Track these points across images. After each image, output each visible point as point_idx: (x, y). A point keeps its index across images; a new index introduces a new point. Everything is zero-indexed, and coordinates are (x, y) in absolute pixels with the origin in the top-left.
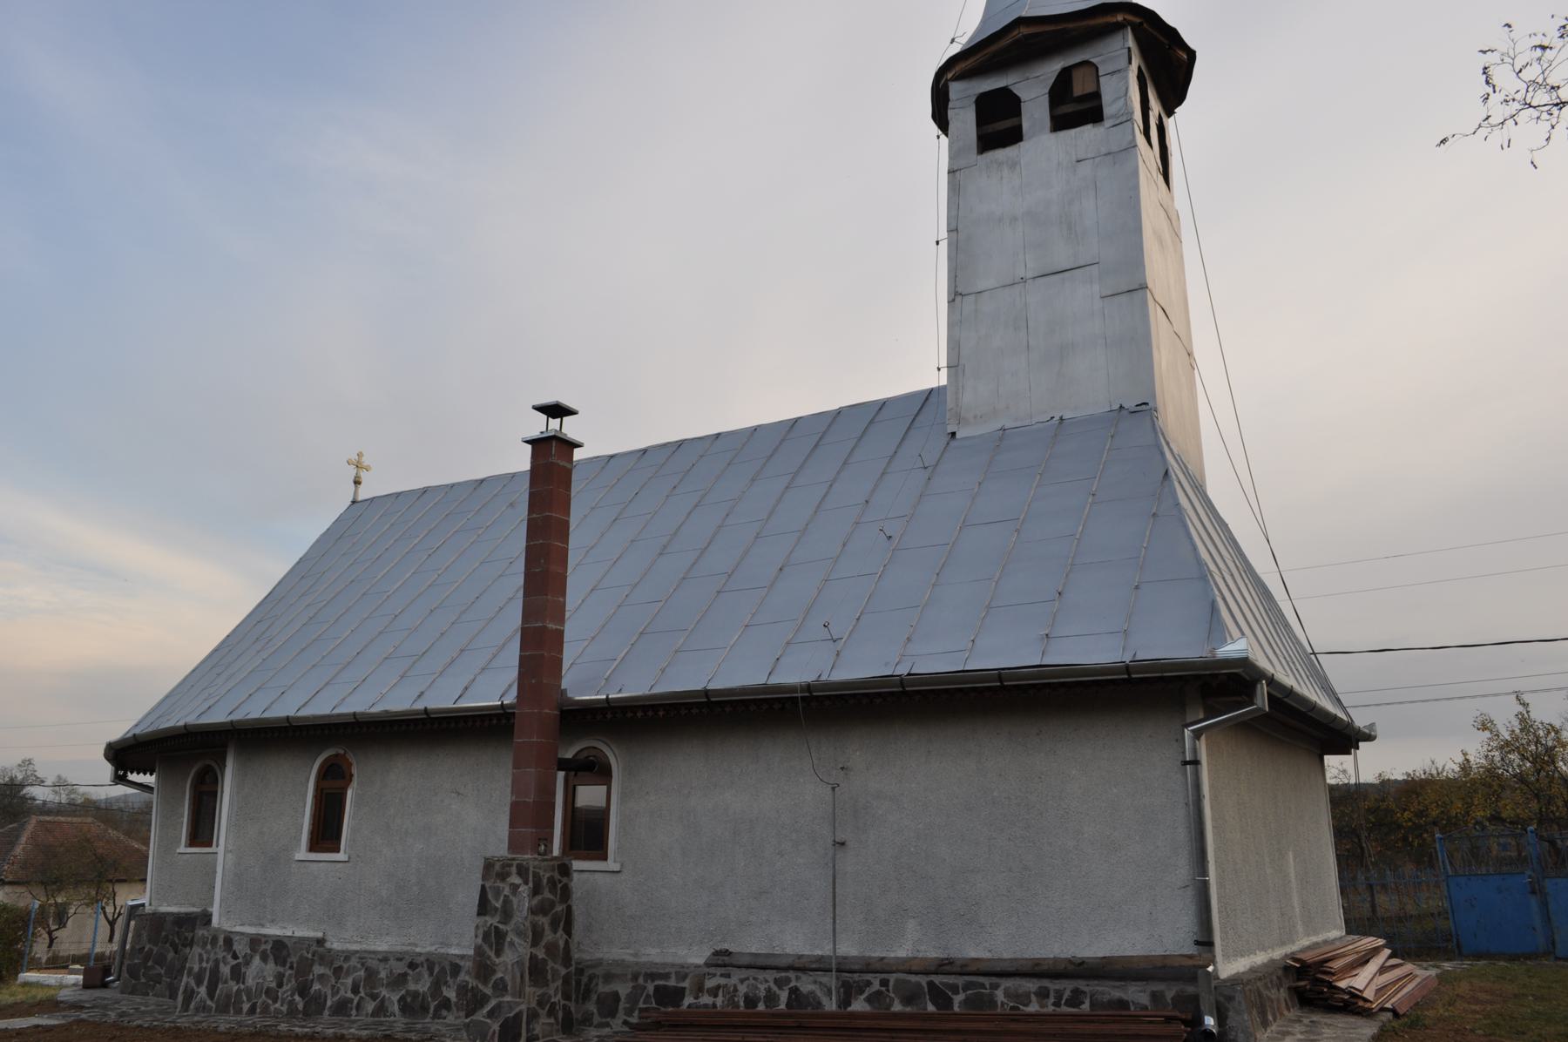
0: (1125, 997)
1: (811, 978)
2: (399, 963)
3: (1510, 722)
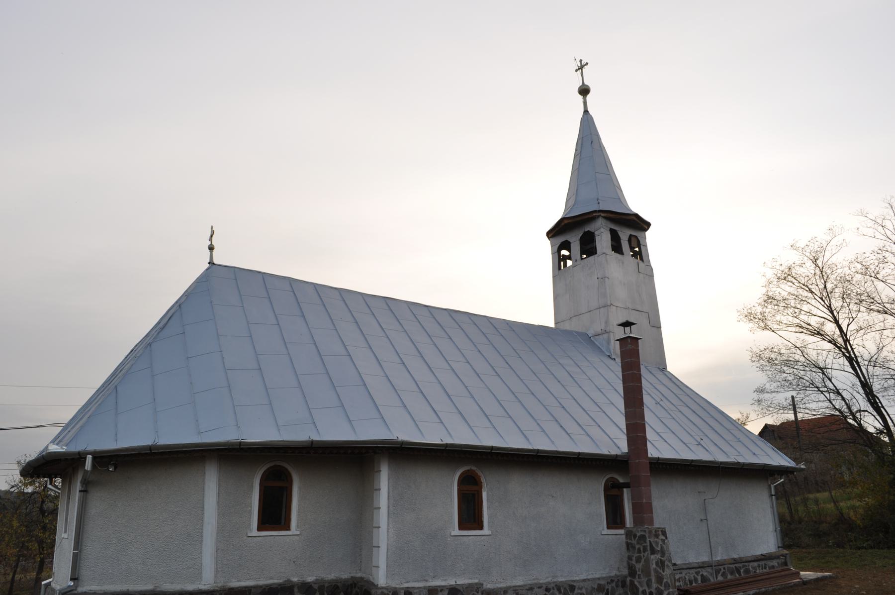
2: (540, 589)
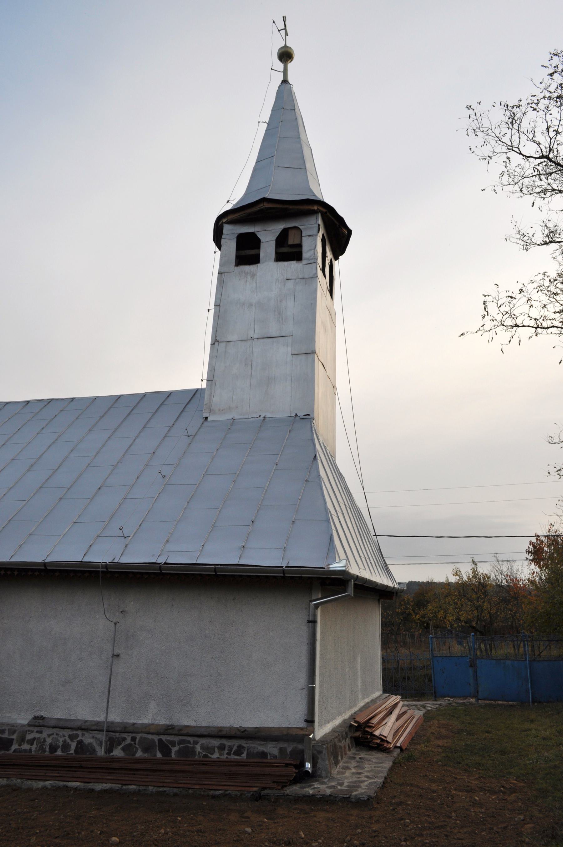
0: (266, 751)
1: (91, 735)
3: (468, 573)
